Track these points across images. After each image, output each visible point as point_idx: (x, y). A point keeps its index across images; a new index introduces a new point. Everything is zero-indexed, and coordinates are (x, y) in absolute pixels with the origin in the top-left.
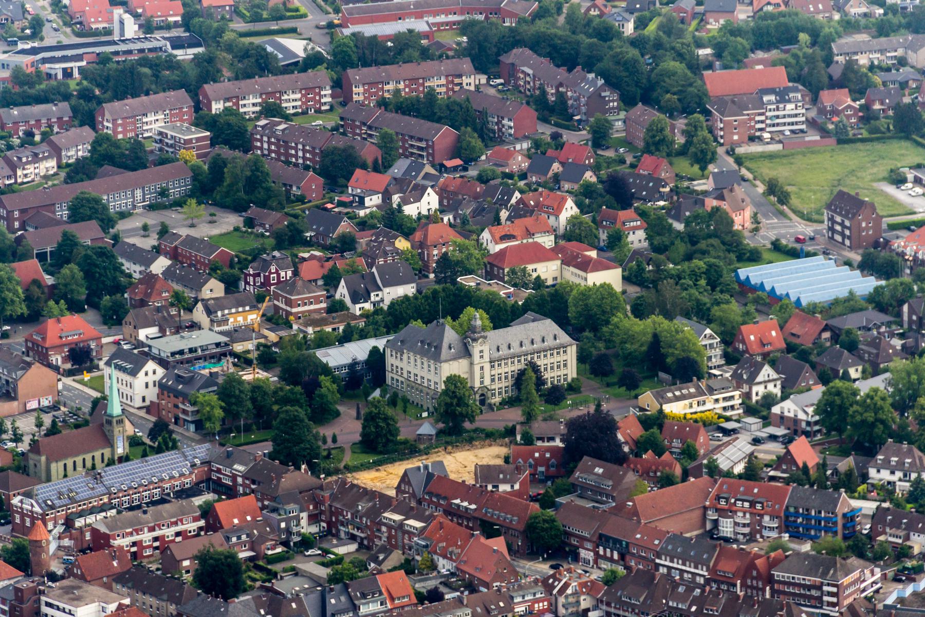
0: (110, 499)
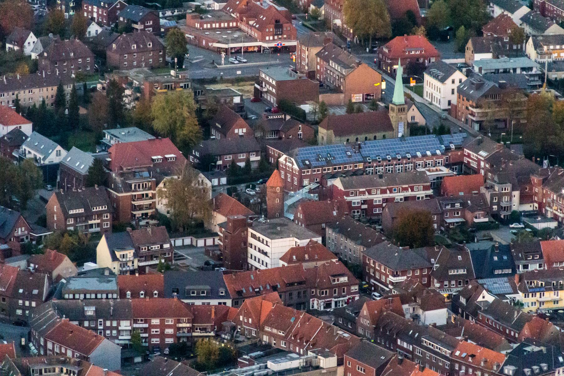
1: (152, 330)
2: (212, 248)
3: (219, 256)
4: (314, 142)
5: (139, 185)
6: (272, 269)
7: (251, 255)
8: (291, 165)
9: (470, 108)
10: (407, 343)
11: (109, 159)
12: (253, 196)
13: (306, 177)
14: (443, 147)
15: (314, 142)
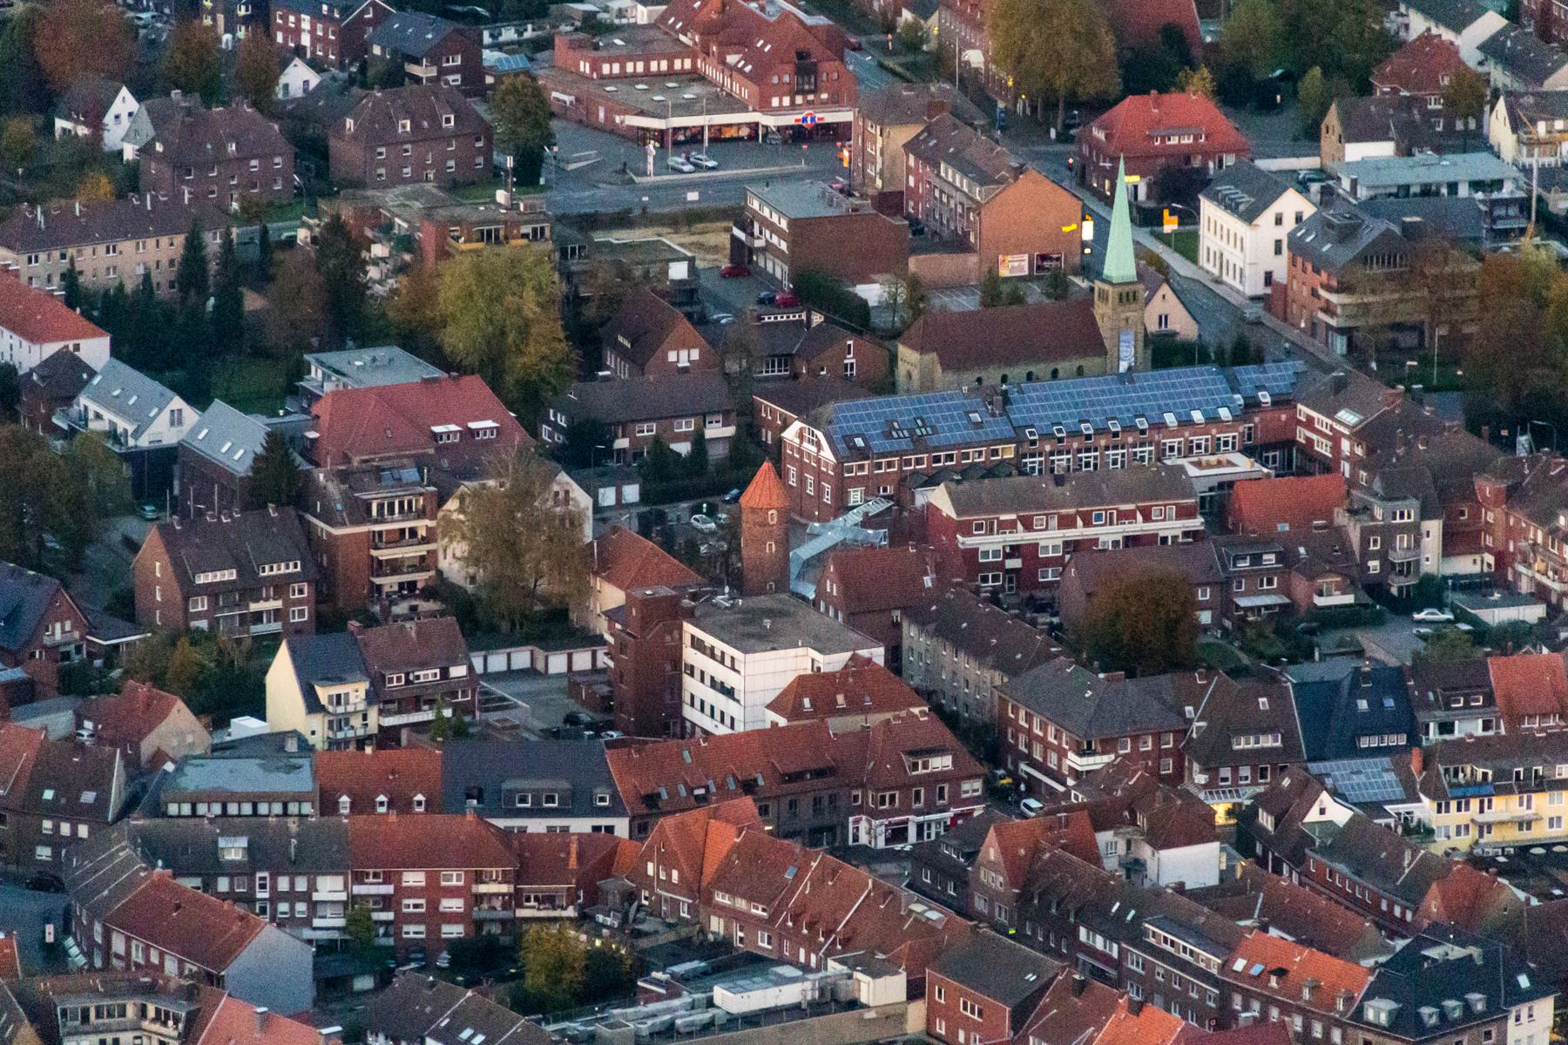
0: (1020, 456)
1: (406, 901)
4: (885, 384)
5: (391, 506)
7: (692, 697)
8: (814, 449)
9: (1322, 292)
11: (312, 435)
13: (857, 482)
14: (1239, 399)
15: (885, 384)
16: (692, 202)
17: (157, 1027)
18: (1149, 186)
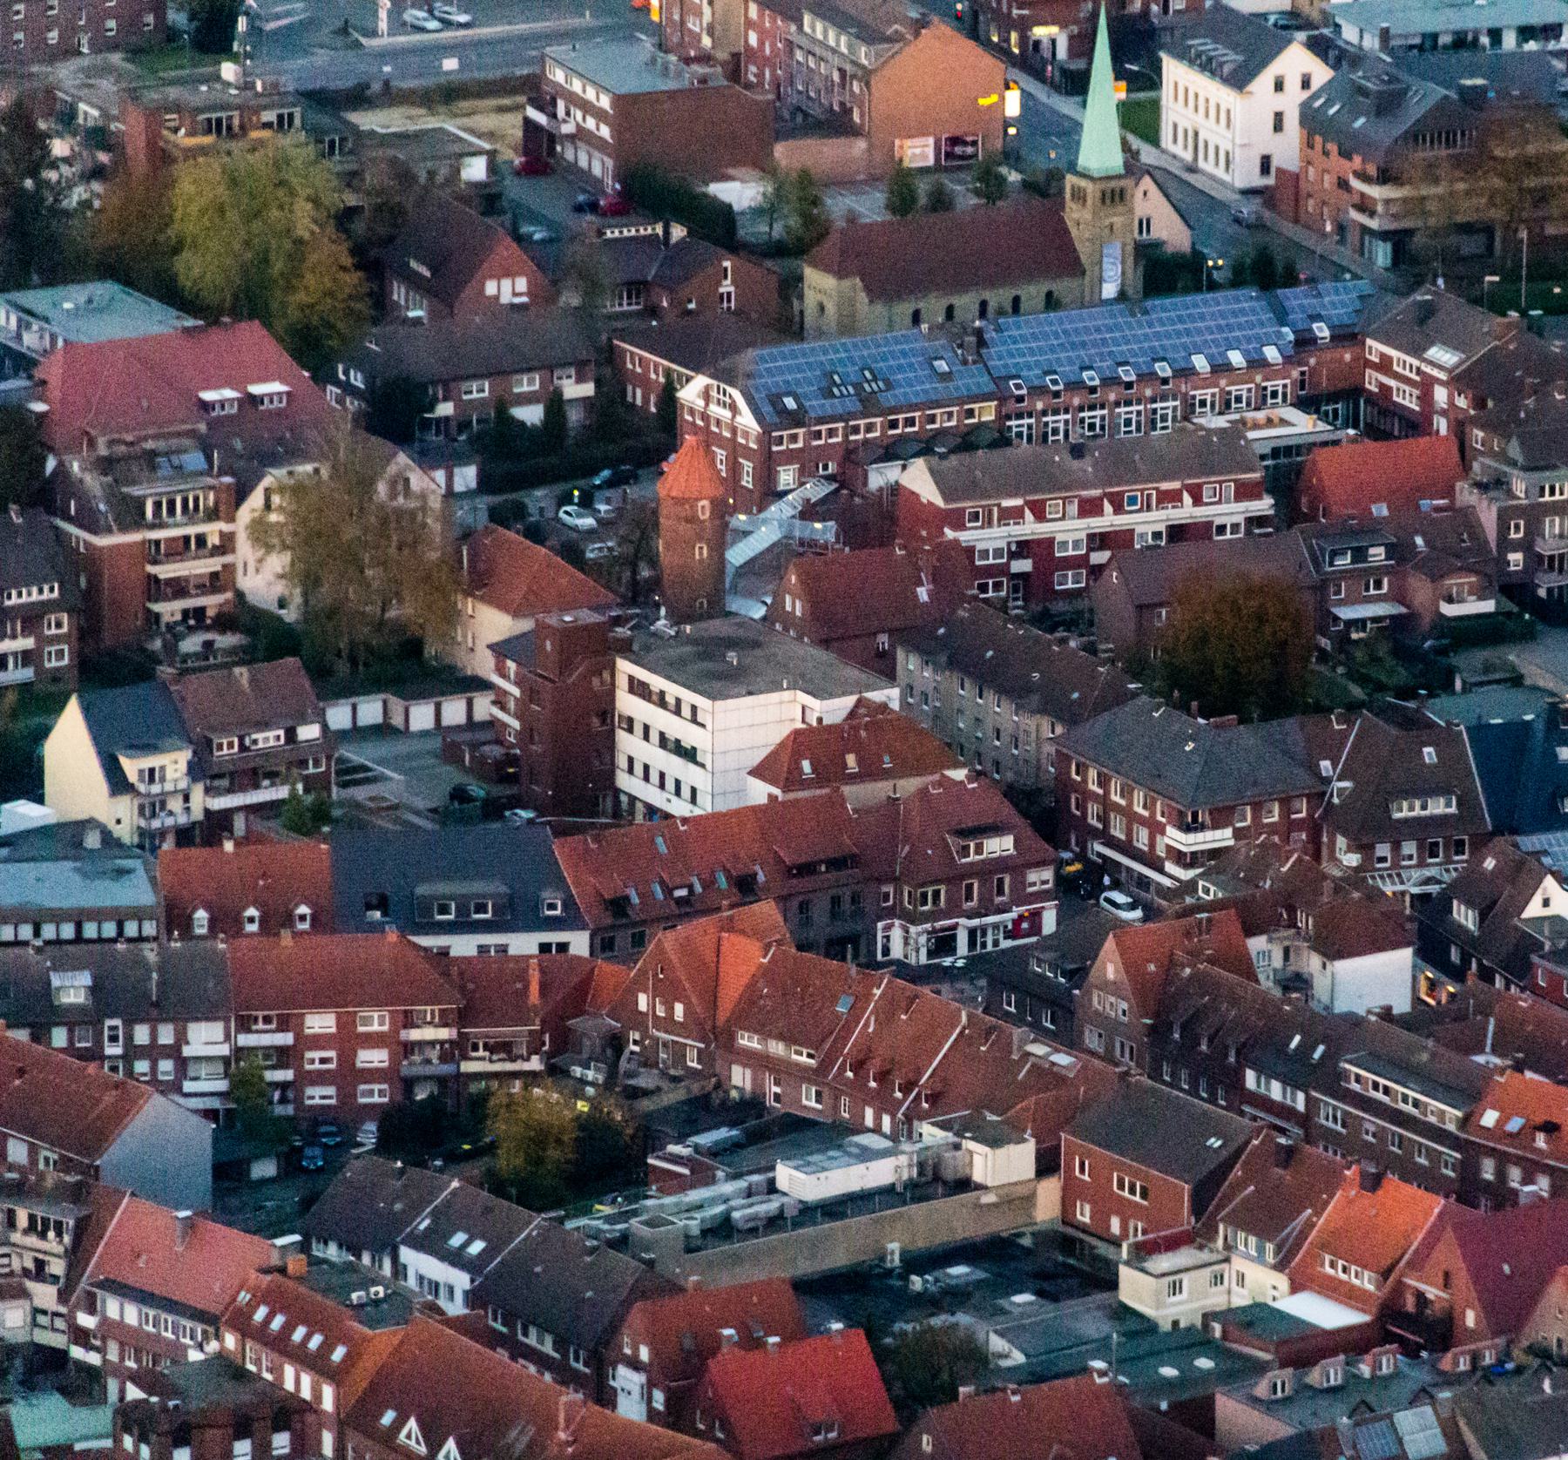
0: (1003, 417)
1: (309, 1055)
2: (467, 736)
3: (500, 765)
4: (790, 327)
5: (171, 504)
6: (715, 816)
7: (631, 760)
8: (726, 414)
9: (1356, 184)
10: (1286, 1081)
11: (39, 407)
12: (590, 534)
13: (790, 457)
14: (1288, 333)
15: (790, 327)
16: (451, 72)
17: (32, 1241)
18: (1071, 38)
